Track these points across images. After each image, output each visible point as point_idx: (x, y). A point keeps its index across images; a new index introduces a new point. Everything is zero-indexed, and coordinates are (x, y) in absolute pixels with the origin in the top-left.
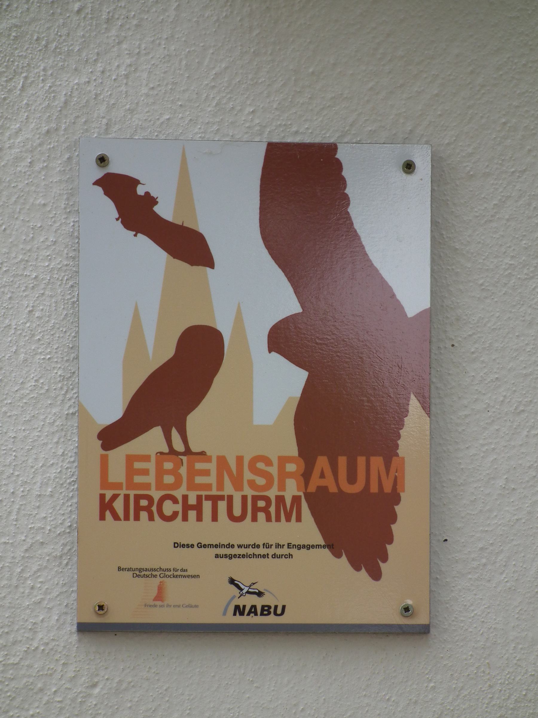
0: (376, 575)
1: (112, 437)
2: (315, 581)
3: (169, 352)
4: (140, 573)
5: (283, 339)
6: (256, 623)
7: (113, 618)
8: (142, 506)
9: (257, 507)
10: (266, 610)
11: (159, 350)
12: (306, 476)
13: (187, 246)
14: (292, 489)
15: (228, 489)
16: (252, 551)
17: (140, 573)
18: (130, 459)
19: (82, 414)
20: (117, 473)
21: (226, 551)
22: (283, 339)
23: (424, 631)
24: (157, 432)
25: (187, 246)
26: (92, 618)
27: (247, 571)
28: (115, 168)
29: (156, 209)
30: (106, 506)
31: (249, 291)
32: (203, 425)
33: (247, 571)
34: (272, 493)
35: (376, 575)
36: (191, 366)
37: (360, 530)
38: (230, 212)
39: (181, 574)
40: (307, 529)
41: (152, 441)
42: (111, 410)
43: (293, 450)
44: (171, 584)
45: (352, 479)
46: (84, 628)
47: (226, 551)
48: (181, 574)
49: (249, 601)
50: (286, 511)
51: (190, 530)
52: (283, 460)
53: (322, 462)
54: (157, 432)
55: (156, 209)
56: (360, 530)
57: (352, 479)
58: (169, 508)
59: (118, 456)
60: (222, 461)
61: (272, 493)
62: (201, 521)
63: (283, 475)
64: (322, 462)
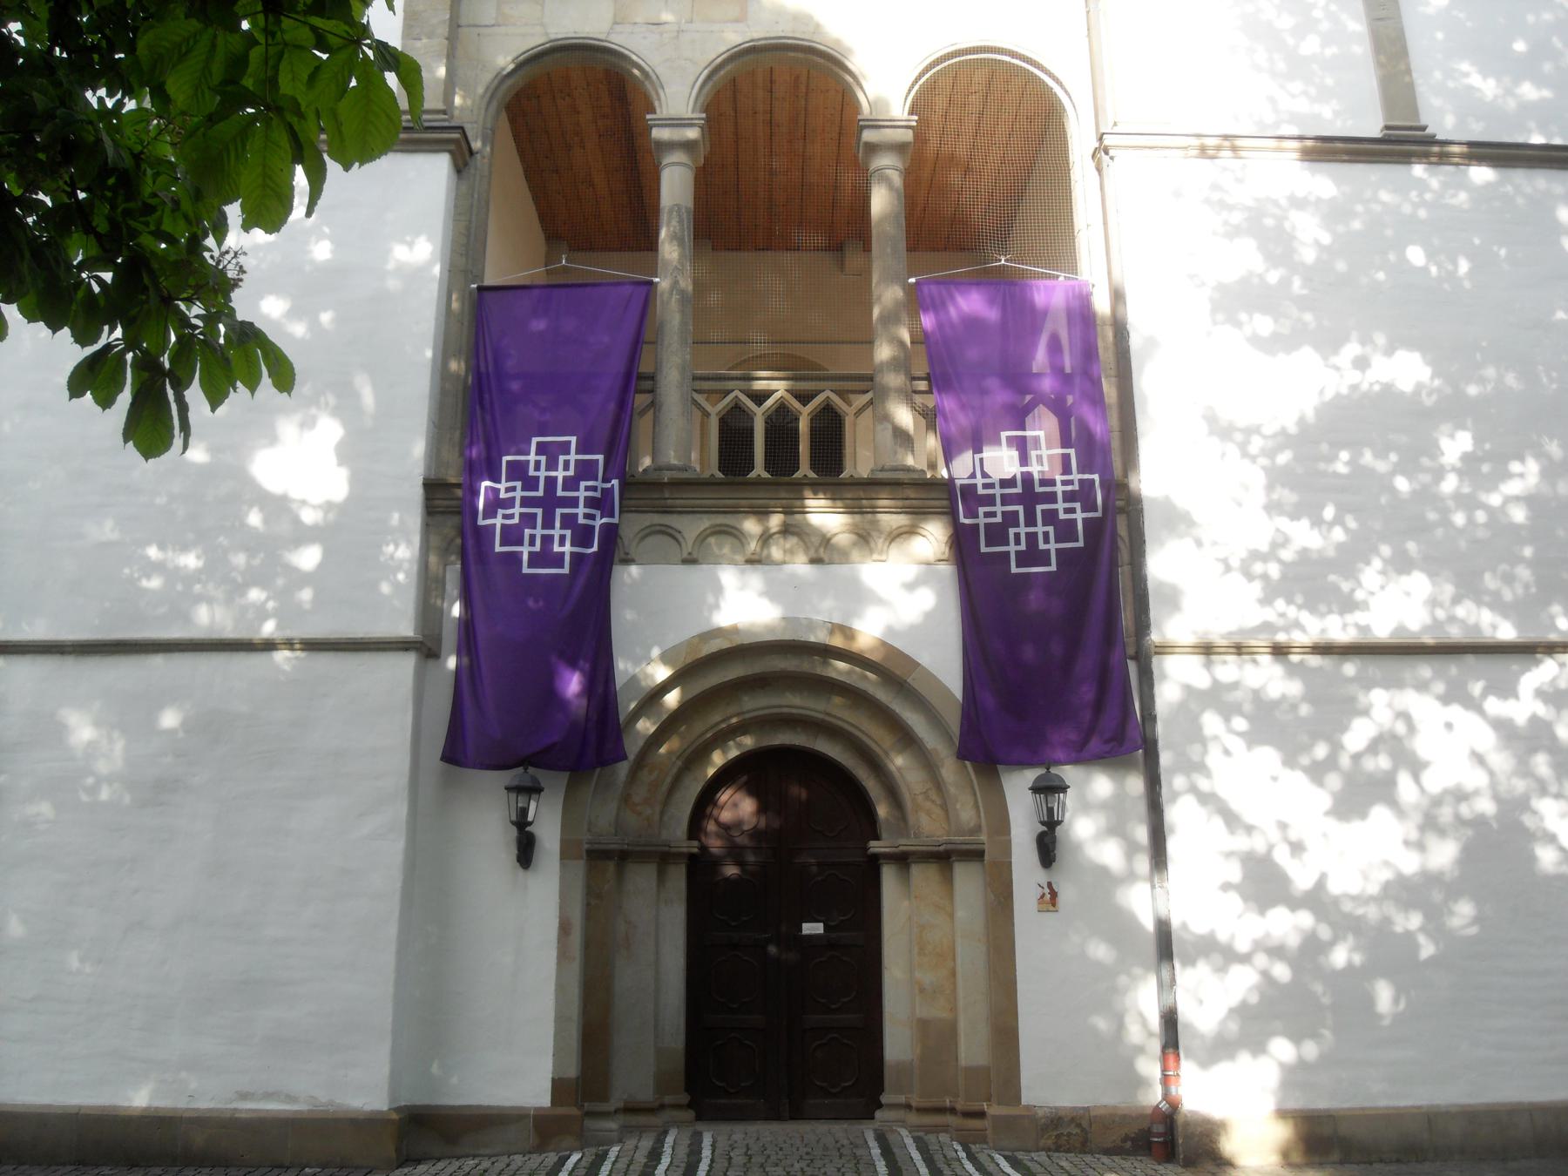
31: (1047, 891)
56: (1054, 905)
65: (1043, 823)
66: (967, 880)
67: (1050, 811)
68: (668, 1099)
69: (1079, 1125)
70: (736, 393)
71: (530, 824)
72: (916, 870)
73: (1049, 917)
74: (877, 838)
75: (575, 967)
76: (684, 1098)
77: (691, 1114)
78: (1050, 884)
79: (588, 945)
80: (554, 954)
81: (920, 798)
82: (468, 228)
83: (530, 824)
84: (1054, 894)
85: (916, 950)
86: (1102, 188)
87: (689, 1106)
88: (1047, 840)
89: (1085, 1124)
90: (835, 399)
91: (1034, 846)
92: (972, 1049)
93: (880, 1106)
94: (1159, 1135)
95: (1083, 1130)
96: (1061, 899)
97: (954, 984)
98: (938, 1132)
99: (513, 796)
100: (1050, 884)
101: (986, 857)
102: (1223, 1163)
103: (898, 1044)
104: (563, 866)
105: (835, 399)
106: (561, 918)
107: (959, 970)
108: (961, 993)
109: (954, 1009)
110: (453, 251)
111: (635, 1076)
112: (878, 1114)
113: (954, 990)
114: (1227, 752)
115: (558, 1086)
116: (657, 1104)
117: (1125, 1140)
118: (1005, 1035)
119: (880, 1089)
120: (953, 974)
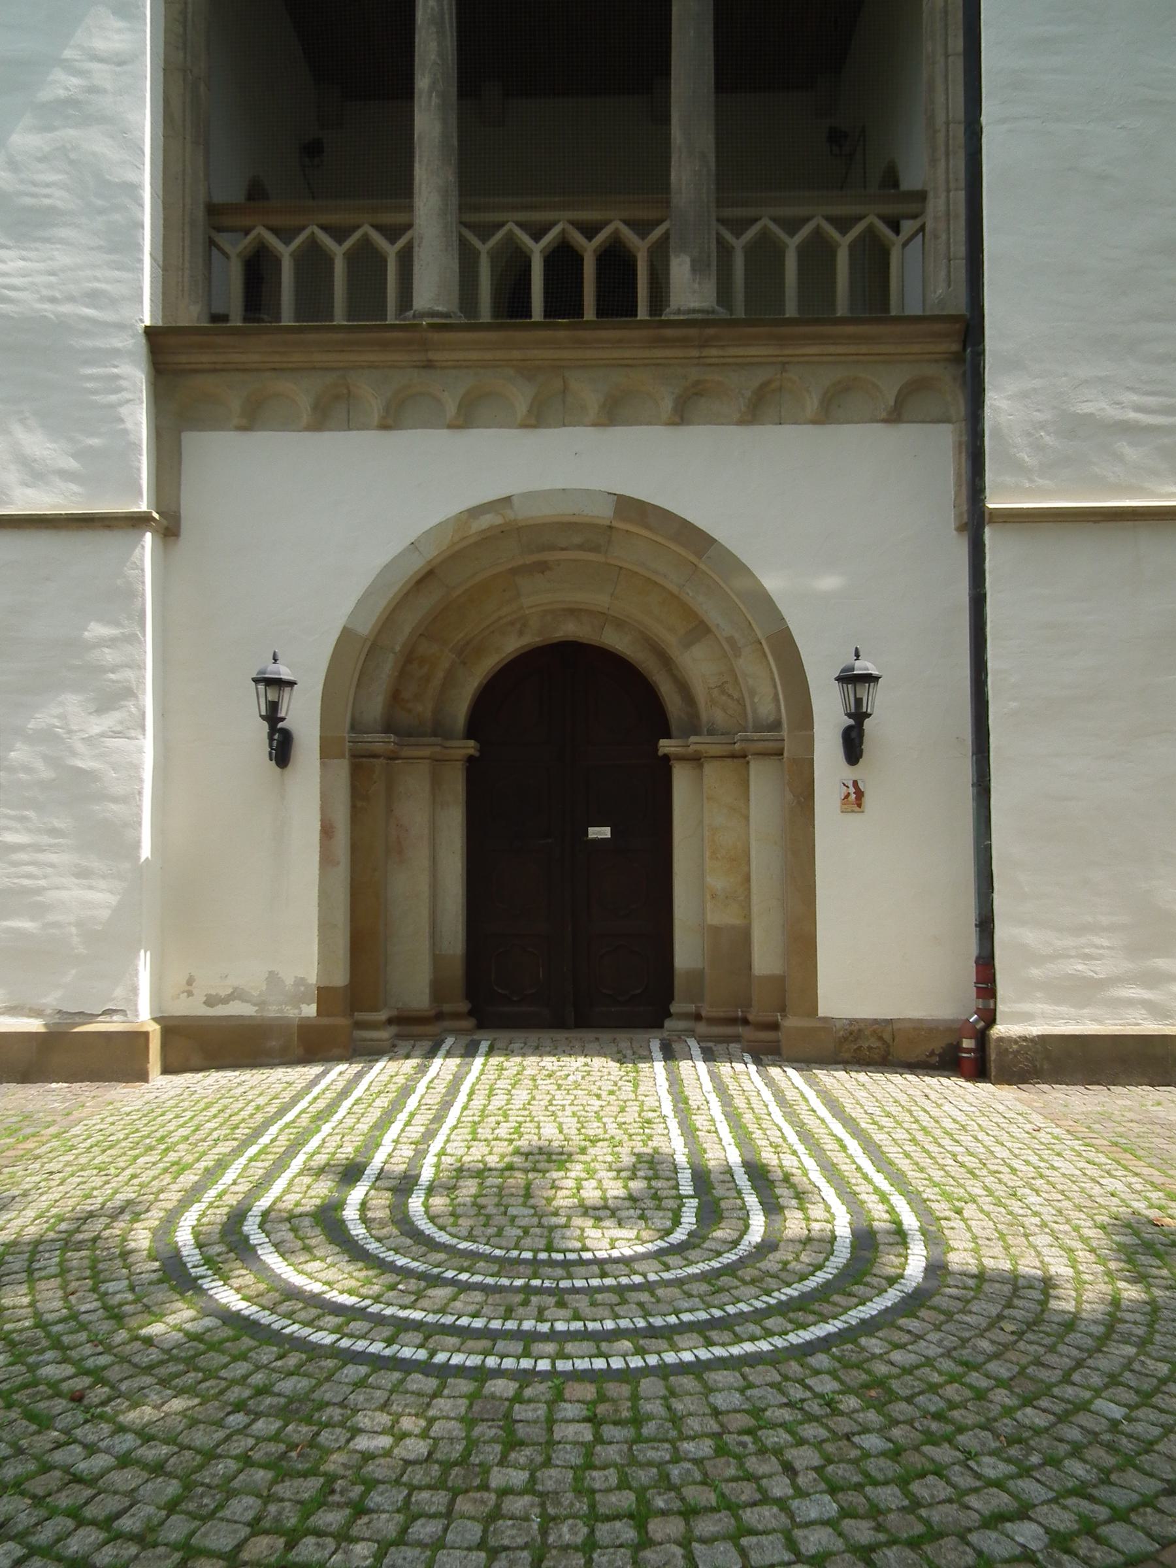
2: (857, 809)
6: (853, 811)
31: (852, 790)
38: (850, 784)
56: (859, 806)
65: (849, 715)
66: (764, 782)
67: (858, 701)
68: (447, 1008)
69: (881, 1038)
70: (765, 221)
71: (283, 719)
72: (709, 768)
73: (854, 819)
74: (668, 736)
75: (342, 872)
76: (463, 1006)
77: (469, 1023)
78: (855, 783)
79: (355, 847)
80: (316, 858)
81: (716, 692)
82: (184, 12)
83: (283, 719)
84: (860, 794)
85: (708, 854)
86: (986, 925)
87: (471, 1013)
88: (854, 734)
89: (887, 1036)
90: (627, 233)
91: (839, 741)
92: (765, 960)
93: (669, 1015)
94: (968, 1051)
95: (885, 1042)
96: (868, 800)
97: (749, 889)
98: (728, 1042)
99: (261, 687)
100: (855, 783)
101: (786, 754)
102: (166, 2)
103: (687, 953)
104: (323, 765)
105: (627, 233)
106: (322, 820)
107: (753, 877)
108: (755, 898)
109: (748, 916)
110: (167, 43)
111: (413, 985)
112: (668, 1024)
113: (748, 897)
114: (952, 1228)
115: (324, 995)
116: (433, 1013)
117: (932, 1053)
118: (802, 943)
119: (670, 998)
120: (748, 879)
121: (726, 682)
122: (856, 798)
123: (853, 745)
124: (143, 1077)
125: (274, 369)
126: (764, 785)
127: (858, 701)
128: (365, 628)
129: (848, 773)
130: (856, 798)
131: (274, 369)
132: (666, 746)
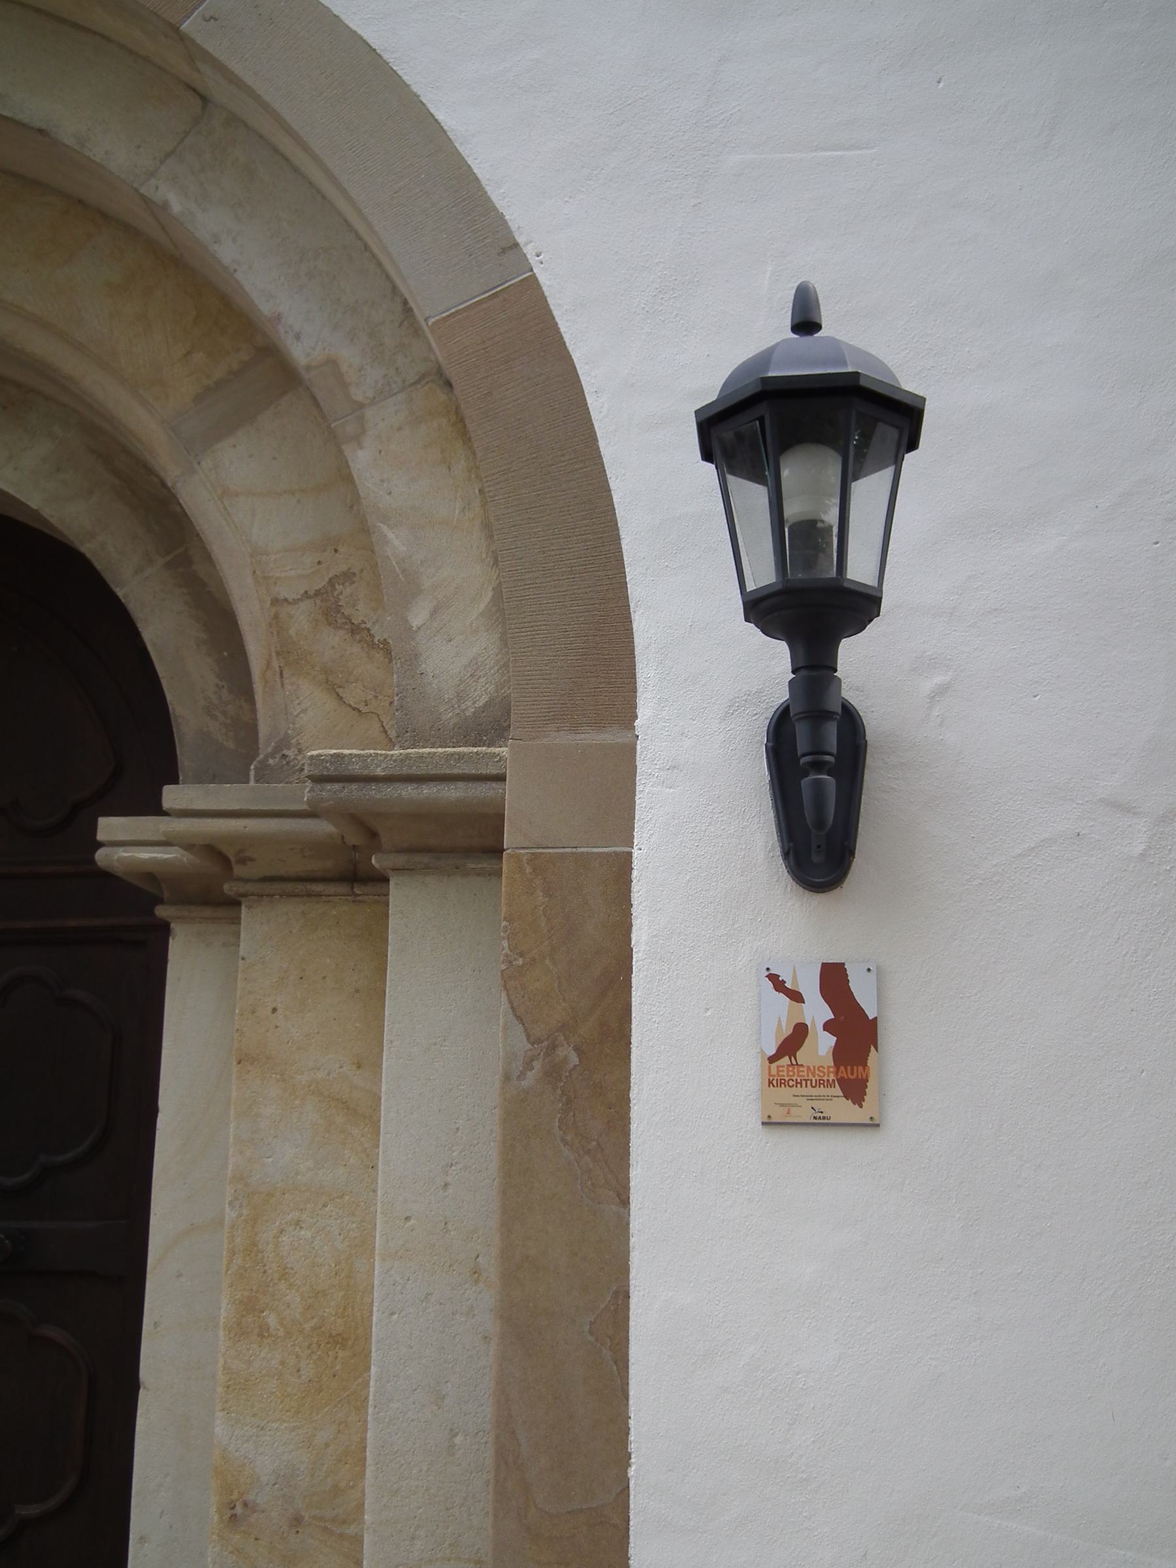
0: (861, 1106)
1: (772, 1059)
2: (841, 1109)
3: (790, 1031)
4: (782, 1105)
5: (828, 1027)
6: (821, 1123)
7: (773, 1120)
8: (782, 1083)
9: (820, 1083)
10: (824, 1118)
11: (787, 1031)
12: (837, 1073)
13: (796, 996)
14: (832, 1077)
15: (811, 1077)
16: (819, 1098)
17: (782, 1105)
18: (778, 1067)
19: (762, 1052)
20: (774, 1071)
21: (810, 1098)
22: (828, 1027)
23: (878, 1125)
24: (787, 1058)
25: (796, 996)
26: (766, 1120)
27: (817, 1105)
28: (772, 972)
29: (830, 1015)
30: (770, 1083)
31: (817, 1011)
32: (802, 1055)
33: (817, 1105)
34: (825, 1078)
35: (861, 1106)
36: (800, 1033)
37: (855, 1090)
38: (810, 986)
39: (796, 1105)
40: (837, 1090)
41: (785, 1061)
42: (772, 1051)
43: (832, 1064)
44: (793, 1109)
45: (852, 1074)
46: (763, 1123)
47: (810, 1098)
48: (796, 1105)
49: (818, 1115)
50: (830, 1084)
51: (798, 1090)
52: (829, 1067)
53: (842, 1068)
54: (787, 1058)
55: (830, 1015)
56: (855, 1090)
57: (852, 1074)
58: (791, 1083)
59: (774, 1065)
60: (808, 1068)
61: (825, 1078)
62: (825, 966)
63: (829, 1072)
64: (842, 1068)
73: (828, 1165)
78: (834, 979)
81: (300, 619)
84: (856, 1034)
96: (897, 1061)
100: (834, 979)
121: (348, 577)
122: (838, 1049)
123: (821, 791)
124: (247, 782)
125: (163, 228)
126: (439, 998)
127: (802, 541)
128: (863, 383)
129: (797, 931)
130: (838, 1049)
131: (163, 228)
132: (127, 842)
